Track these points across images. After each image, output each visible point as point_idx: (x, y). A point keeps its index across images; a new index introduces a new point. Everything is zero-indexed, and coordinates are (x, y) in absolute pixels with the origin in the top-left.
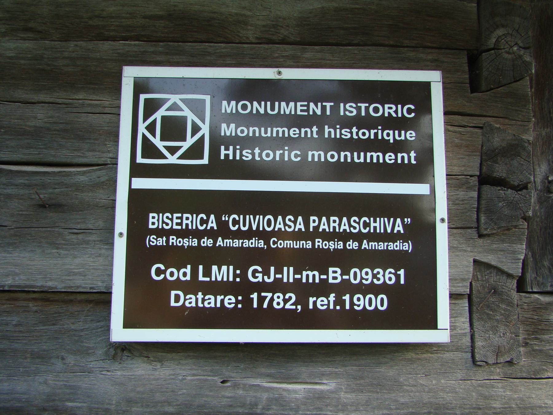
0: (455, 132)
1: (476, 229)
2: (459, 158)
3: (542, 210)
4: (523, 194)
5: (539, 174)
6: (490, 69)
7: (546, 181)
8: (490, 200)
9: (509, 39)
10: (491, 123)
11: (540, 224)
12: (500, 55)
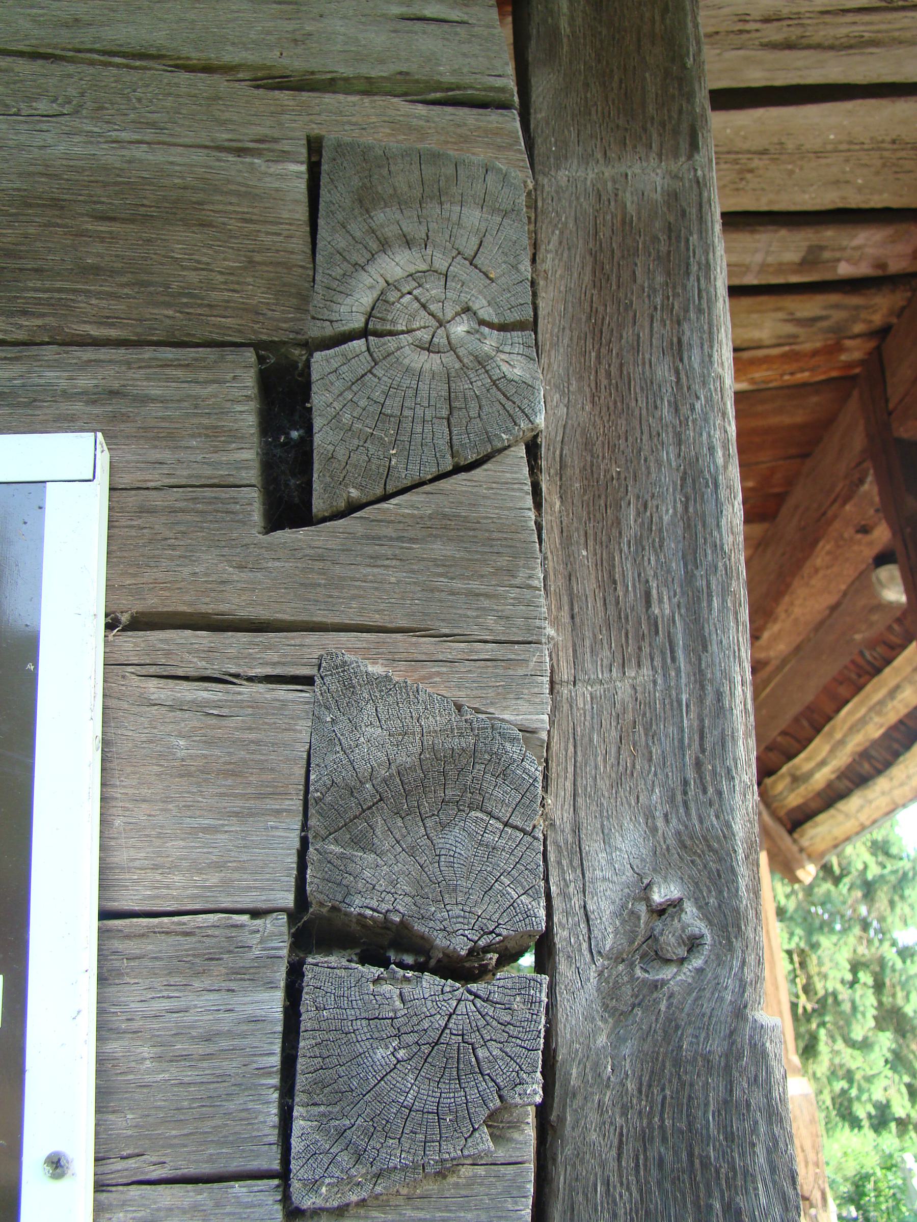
0: (178, 707)
1: (276, 1182)
2: (193, 832)
3: (627, 1050)
4: (496, 997)
5: (604, 879)
6: (346, 418)
7: (642, 908)
8: (331, 1036)
9: (433, 292)
10: (348, 657)
11: (619, 1121)
12: (392, 359)
